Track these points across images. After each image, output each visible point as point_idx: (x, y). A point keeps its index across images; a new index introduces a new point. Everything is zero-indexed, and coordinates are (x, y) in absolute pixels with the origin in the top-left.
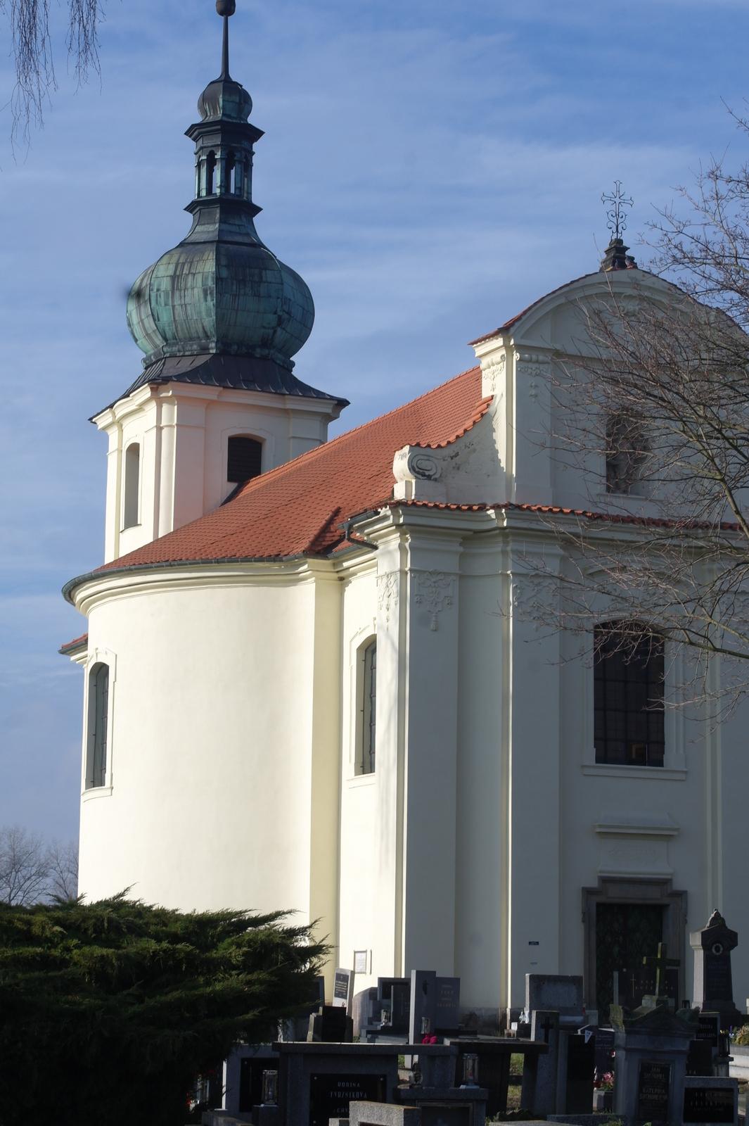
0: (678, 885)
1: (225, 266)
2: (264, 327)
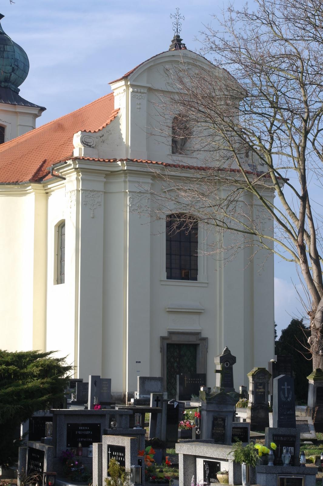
0: (204, 335)
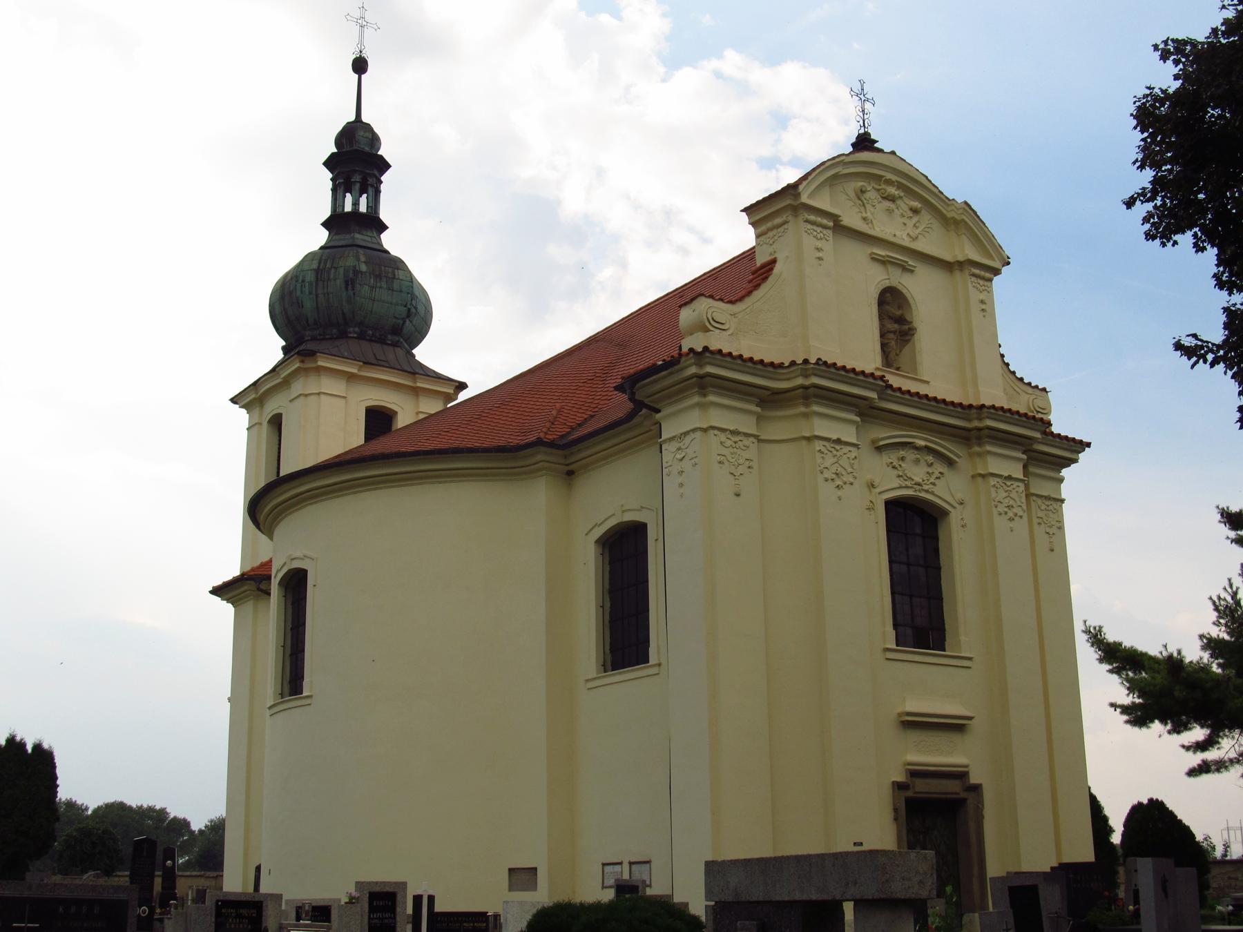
0: (974, 779)
1: (364, 262)
2: (395, 318)
